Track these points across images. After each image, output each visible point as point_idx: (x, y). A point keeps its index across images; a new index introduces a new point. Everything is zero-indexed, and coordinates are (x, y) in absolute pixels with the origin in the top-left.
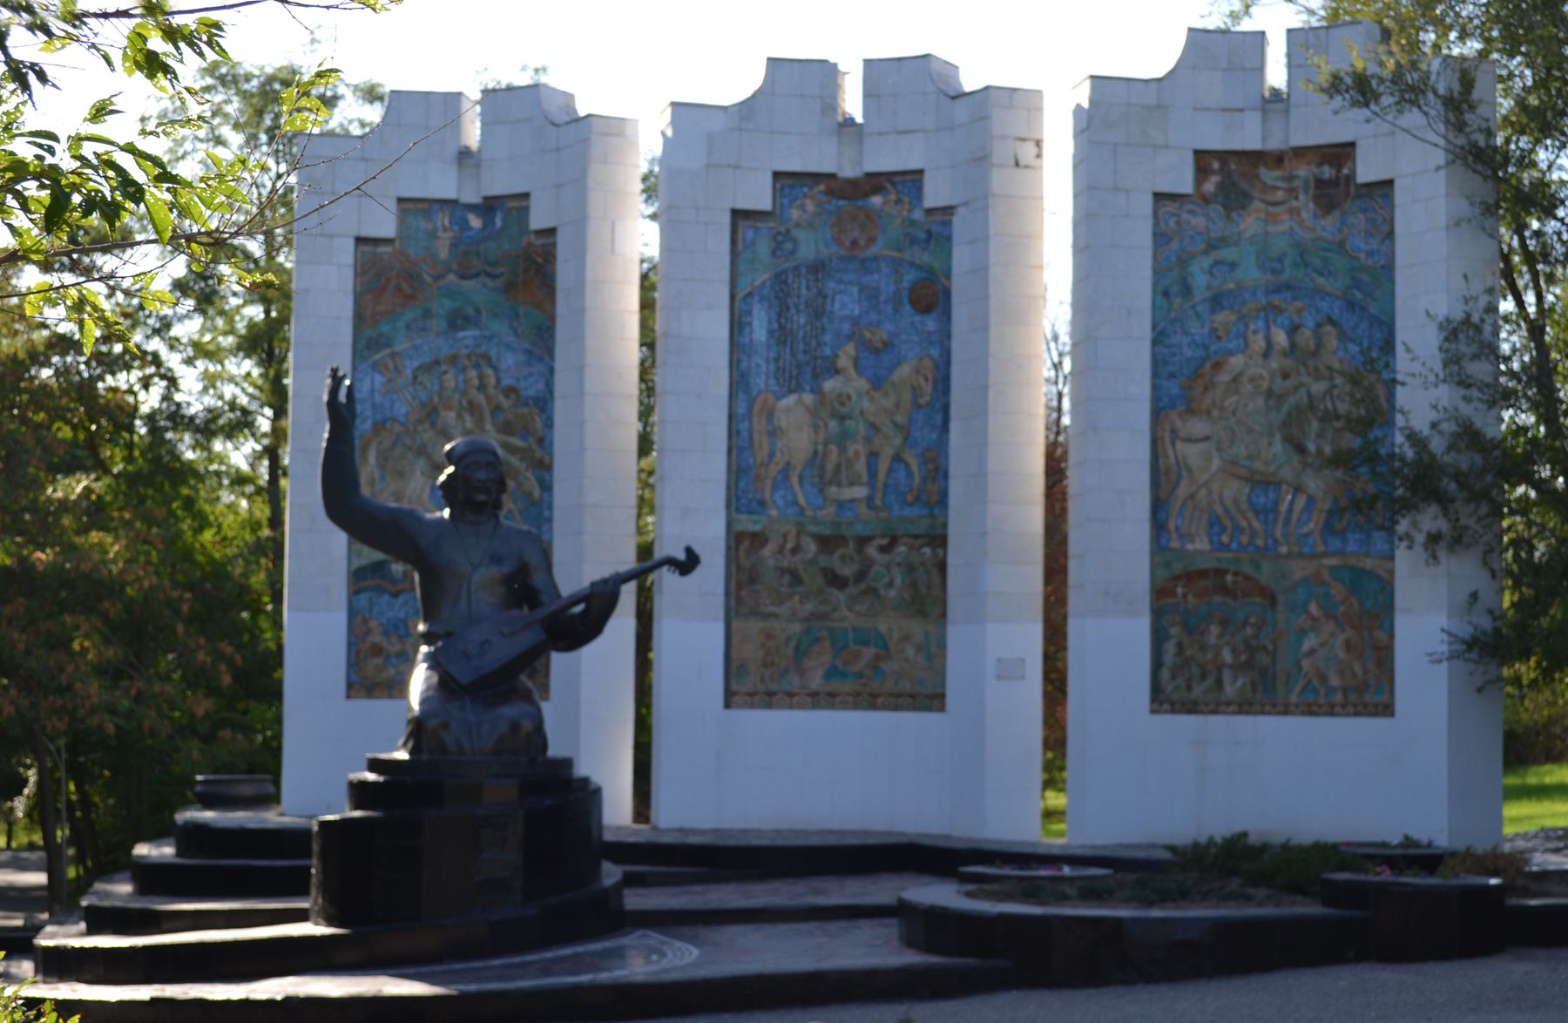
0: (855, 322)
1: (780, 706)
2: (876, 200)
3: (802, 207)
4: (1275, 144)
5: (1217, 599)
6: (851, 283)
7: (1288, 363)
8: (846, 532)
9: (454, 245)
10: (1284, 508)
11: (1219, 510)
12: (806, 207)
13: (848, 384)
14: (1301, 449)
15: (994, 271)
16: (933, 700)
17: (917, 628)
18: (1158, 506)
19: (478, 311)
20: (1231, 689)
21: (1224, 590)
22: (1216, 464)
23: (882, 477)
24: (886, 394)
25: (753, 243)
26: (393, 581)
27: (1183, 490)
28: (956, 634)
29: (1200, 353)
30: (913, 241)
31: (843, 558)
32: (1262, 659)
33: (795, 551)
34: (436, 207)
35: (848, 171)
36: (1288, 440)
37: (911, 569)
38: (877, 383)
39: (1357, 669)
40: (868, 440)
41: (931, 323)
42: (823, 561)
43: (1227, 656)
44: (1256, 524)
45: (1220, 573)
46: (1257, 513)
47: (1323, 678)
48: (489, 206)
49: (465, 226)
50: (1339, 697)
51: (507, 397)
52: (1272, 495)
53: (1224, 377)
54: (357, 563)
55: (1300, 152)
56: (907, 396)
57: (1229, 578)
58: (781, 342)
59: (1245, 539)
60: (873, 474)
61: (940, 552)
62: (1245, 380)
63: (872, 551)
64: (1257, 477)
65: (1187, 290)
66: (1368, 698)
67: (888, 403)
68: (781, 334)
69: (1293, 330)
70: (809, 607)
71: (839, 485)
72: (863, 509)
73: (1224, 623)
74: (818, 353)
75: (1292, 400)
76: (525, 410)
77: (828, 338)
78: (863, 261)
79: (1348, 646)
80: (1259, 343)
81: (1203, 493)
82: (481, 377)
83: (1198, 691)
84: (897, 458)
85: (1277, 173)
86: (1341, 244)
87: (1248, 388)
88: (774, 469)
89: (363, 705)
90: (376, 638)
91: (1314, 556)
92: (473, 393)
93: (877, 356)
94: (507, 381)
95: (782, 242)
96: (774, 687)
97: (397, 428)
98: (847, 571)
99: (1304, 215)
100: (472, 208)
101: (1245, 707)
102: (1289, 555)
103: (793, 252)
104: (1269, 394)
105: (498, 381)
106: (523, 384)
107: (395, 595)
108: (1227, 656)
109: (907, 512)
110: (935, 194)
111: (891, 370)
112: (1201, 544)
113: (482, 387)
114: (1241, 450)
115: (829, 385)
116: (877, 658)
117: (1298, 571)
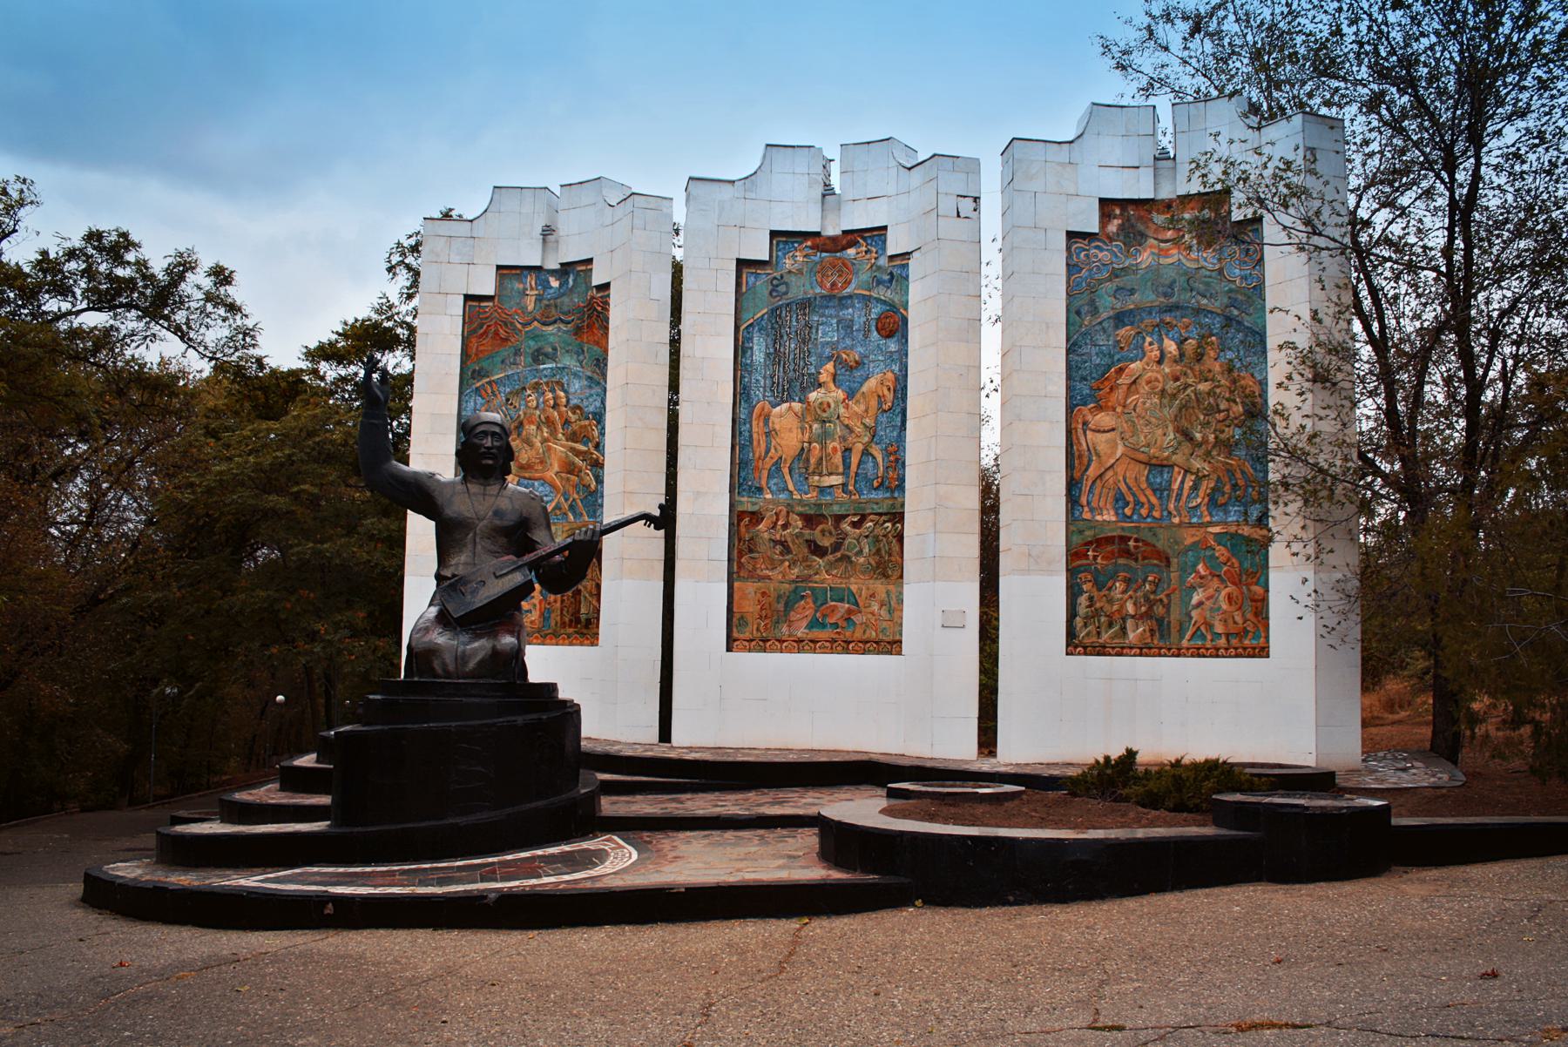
2: (851, 252)
3: (794, 257)
5: (1121, 561)
10: (1176, 486)
13: (827, 395)
18: (1072, 485)
20: (1132, 636)
21: (1127, 553)
29: (1107, 360)
30: (880, 282)
31: (823, 531)
32: (1159, 610)
33: (785, 527)
37: (877, 540)
39: (1238, 619)
41: (893, 346)
44: (1154, 500)
45: (1124, 540)
46: (1154, 491)
47: (1209, 626)
48: (567, 268)
49: (547, 286)
50: (1222, 642)
53: (1124, 380)
56: (874, 403)
57: (1131, 543)
59: (1144, 512)
60: (847, 466)
63: (846, 526)
65: (1095, 311)
68: (775, 357)
69: (1181, 343)
71: (820, 475)
73: (1128, 581)
79: (1230, 598)
83: (1105, 637)
84: (866, 452)
88: (769, 463)
93: (850, 371)
94: (574, 401)
98: (826, 542)
100: (553, 272)
101: (1144, 650)
102: (1180, 525)
108: (1130, 608)
112: (1109, 516)
115: (813, 396)
116: (849, 611)
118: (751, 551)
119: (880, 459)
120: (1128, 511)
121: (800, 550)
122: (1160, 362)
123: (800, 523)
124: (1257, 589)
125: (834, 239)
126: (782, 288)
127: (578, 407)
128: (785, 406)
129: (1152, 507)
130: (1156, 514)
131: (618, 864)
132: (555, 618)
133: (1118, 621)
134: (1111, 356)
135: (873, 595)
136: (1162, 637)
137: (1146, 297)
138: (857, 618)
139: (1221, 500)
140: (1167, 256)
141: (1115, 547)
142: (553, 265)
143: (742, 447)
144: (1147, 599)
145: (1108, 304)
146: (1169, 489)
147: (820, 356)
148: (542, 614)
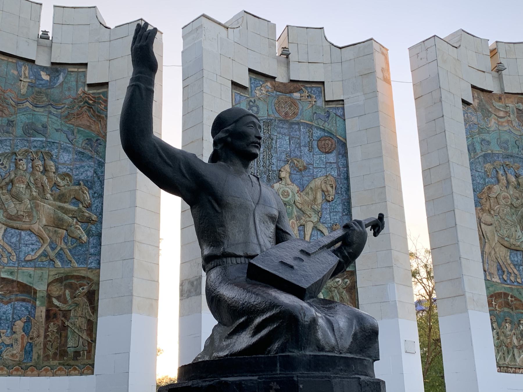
2: (297, 95)
5: (506, 310)
6: (285, 134)
9: (31, 86)
19: (45, 127)
21: (508, 305)
24: (307, 194)
34: (21, 63)
38: (302, 188)
41: (332, 158)
44: (515, 271)
48: (56, 67)
49: (38, 78)
51: (63, 179)
56: (319, 195)
64: (513, 247)
73: (511, 323)
74: (270, 168)
76: (77, 187)
78: (293, 123)
82: (45, 166)
84: (315, 228)
85: (500, 104)
92: (38, 175)
94: (63, 170)
100: (44, 68)
105: (57, 169)
110: (332, 92)
111: (309, 182)
113: (45, 171)
114: (504, 232)
127: (68, 175)
132: (37, 351)
142: (43, 61)
147: (279, 160)
148: (24, 348)
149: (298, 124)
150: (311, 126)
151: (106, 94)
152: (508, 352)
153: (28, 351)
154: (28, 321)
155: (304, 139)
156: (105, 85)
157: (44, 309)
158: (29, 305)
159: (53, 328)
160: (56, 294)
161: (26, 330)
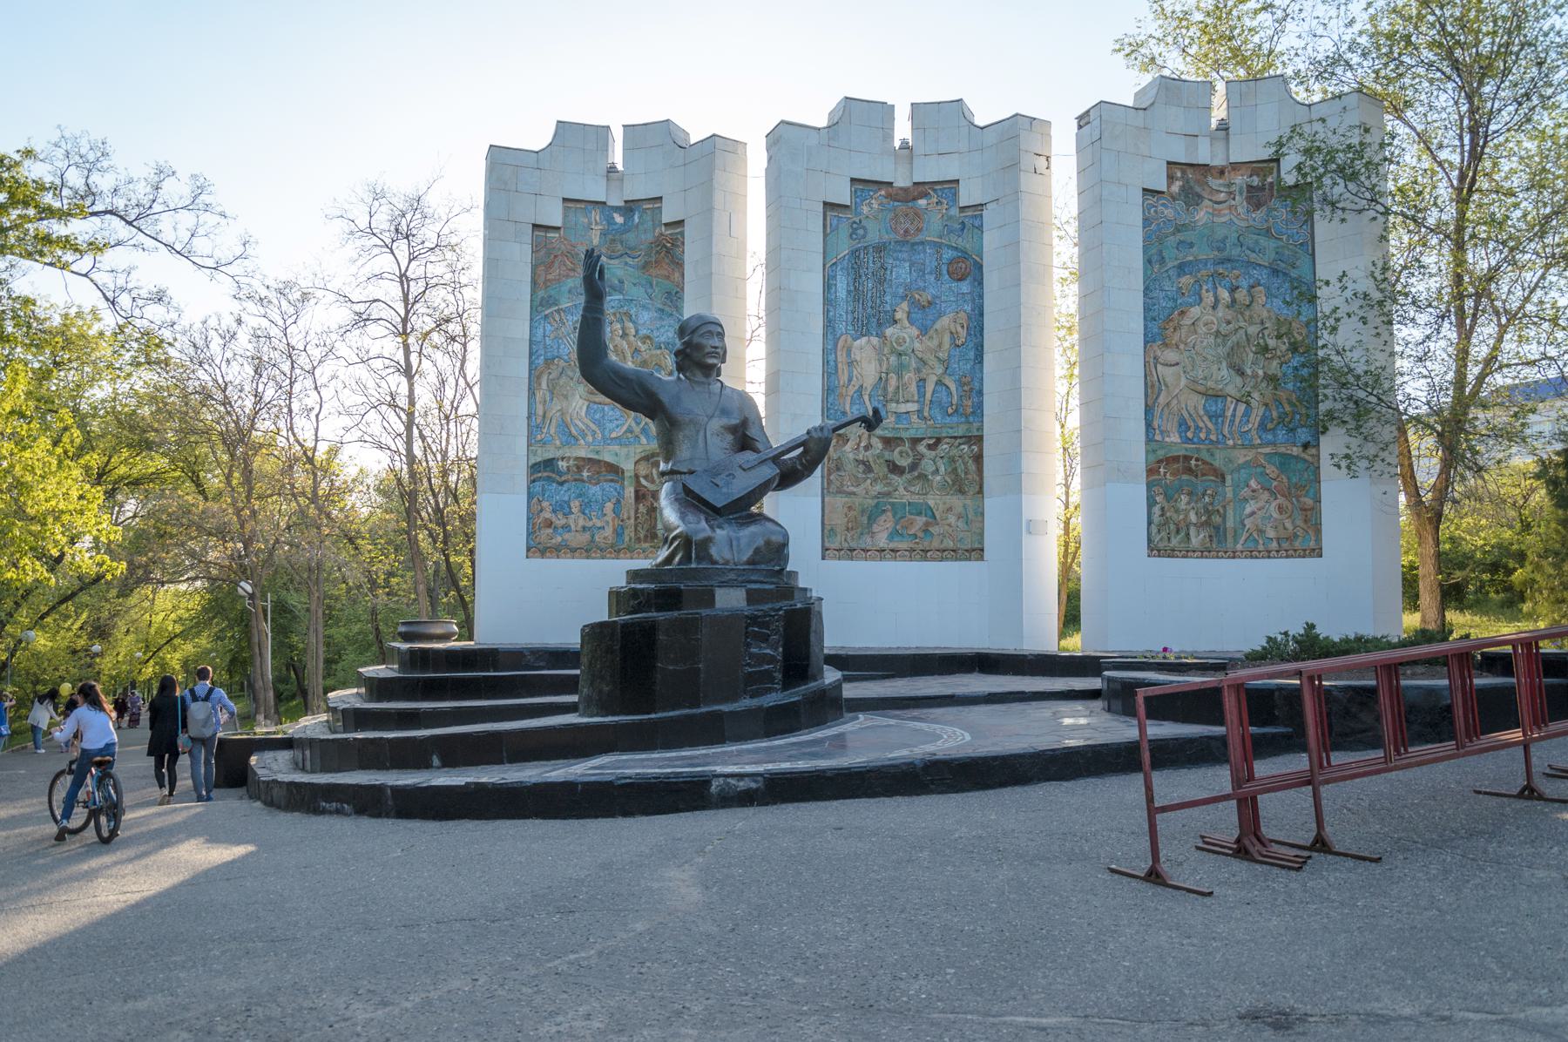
0: (908, 287)
1: (858, 559)
2: (922, 202)
3: (870, 204)
4: (1218, 161)
5: (1185, 477)
7: (1230, 314)
8: (904, 435)
9: (604, 234)
10: (1229, 413)
11: (1186, 415)
12: (872, 205)
13: (903, 332)
14: (1241, 373)
15: (1024, 245)
16: (976, 552)
17: (957, 502)
18: (1149, 410)
19: (621, 282)
20: (1195, 541)
21: (1189, 470)
22: (1183, 382)
23: (928, 396)
25: (837, 228)
26: (560, 473)
27: (1162, 400)
28: (990, 504)
29: (1170, 304)
30: (951, 232)
31: (901, 453)
32: (1216, 519)
33: (867, 448)
34: (590, 207)
35: (902, 182)
36: (1232, 366)
37: (952, 460)
38: (924, 330)
39: (1289, 525)
40: (918, 370)
41: (965, 287)
42: (887, 455)
43: (1193, 517)
44: (1210, 425)
45: (1187, 458)
46: (1210, 417)
47: (1261, 532)
48: (630, 207)
49: (610, 221)
50: (1274, 545)
52: (1220, 406)
53: (1187, 321)
54: (532, 461)
55: (1236, 166)
56: (947, 339)
57: (1193, 462)
58: (856, 300)
59: (1203, 436)
60: (922, 394)
61: (975, 448)
62: (1201, 324)
63: (922, 448)
65: (1162, 261)
66: (1297, 544)
67: (934, 344)
68: (856, 294)
69: (1233, 290)
70: (879, 488)
71: (898, 402)
72: (914, 418)
73: (1190, 494)
75: (1234, 338)
77: (888, 298)
78: (914, 244)
79: (1280, 509)
80: (1209, 298)
81: (1175, 402)
82: (623, 329)
83: (1174, 542)
84: (939, 383)
86: (1268, 230)
87: (1202, 329)
88: (852, 390)
89: (537, 563)
90: (547, 515)
91: (1253, 446)
93: (924, 312)
94: (643, 332)
95: (856, 229)
96: (853, 545)
97: (562, 363)
98: (904, 462)
99: (1240, 210)
100: (616, 209)
101: (1205, 552)
102: (1234, 447)
103: (864, 237)
104: (1218, 334)
106: (656, 334)
107: (561, 484)
108: (1193, 517)
109: (948, 420)
112: (1174, 438)
113: (624, 335)
115: (889, 331)
116: (927, 524)
117: (1242, 457)
118: (838, 469)
119: (953, 387)
120: (1190, 435)
121: (880, 469)
122: (1214, 308)
123: (880, 446)
124: (1309, 502)
125: (905, 190)
126: (861, 232)
127: (648, 337)
128: (864, 339)
129: (1209, 432)
130: (1213, 437)
131: (865, 741)
132: (629, 533)
133: (1182, 529)
134: (1175, 301)
135: (950, 509)
136: (1219, 542)
137: (1202, 252)
138: (934, 530)
139: (1270, 426)
140: (1219, 215)
141: (1180, 465)
142: (616, 201)
143: (829, 375)
144: (1207, 511)
145: (1173, 257)
146: (1223, 415)
147: (894, 296)
148: (615, 531)
149: (922, 243)
150: (940, 245)
151: (682, 234)
152: (1178, 532)
153: (618, 533)
154: (618, 501)
155: (930, 263)
156: (681, 223)
157: (632, 490)
158: (618, 486)
159: (642, 509)
160: (643, 473)
161: (616, 512)
